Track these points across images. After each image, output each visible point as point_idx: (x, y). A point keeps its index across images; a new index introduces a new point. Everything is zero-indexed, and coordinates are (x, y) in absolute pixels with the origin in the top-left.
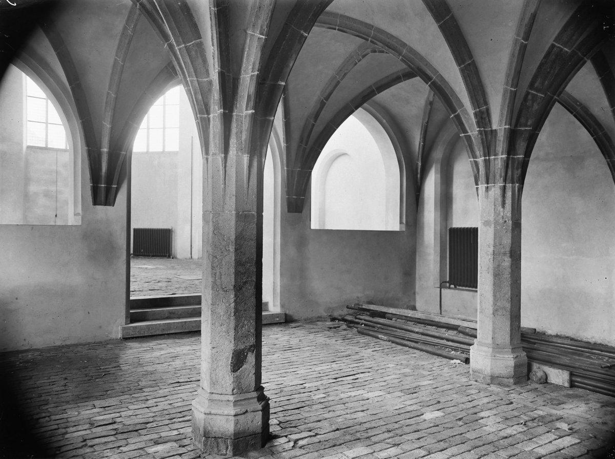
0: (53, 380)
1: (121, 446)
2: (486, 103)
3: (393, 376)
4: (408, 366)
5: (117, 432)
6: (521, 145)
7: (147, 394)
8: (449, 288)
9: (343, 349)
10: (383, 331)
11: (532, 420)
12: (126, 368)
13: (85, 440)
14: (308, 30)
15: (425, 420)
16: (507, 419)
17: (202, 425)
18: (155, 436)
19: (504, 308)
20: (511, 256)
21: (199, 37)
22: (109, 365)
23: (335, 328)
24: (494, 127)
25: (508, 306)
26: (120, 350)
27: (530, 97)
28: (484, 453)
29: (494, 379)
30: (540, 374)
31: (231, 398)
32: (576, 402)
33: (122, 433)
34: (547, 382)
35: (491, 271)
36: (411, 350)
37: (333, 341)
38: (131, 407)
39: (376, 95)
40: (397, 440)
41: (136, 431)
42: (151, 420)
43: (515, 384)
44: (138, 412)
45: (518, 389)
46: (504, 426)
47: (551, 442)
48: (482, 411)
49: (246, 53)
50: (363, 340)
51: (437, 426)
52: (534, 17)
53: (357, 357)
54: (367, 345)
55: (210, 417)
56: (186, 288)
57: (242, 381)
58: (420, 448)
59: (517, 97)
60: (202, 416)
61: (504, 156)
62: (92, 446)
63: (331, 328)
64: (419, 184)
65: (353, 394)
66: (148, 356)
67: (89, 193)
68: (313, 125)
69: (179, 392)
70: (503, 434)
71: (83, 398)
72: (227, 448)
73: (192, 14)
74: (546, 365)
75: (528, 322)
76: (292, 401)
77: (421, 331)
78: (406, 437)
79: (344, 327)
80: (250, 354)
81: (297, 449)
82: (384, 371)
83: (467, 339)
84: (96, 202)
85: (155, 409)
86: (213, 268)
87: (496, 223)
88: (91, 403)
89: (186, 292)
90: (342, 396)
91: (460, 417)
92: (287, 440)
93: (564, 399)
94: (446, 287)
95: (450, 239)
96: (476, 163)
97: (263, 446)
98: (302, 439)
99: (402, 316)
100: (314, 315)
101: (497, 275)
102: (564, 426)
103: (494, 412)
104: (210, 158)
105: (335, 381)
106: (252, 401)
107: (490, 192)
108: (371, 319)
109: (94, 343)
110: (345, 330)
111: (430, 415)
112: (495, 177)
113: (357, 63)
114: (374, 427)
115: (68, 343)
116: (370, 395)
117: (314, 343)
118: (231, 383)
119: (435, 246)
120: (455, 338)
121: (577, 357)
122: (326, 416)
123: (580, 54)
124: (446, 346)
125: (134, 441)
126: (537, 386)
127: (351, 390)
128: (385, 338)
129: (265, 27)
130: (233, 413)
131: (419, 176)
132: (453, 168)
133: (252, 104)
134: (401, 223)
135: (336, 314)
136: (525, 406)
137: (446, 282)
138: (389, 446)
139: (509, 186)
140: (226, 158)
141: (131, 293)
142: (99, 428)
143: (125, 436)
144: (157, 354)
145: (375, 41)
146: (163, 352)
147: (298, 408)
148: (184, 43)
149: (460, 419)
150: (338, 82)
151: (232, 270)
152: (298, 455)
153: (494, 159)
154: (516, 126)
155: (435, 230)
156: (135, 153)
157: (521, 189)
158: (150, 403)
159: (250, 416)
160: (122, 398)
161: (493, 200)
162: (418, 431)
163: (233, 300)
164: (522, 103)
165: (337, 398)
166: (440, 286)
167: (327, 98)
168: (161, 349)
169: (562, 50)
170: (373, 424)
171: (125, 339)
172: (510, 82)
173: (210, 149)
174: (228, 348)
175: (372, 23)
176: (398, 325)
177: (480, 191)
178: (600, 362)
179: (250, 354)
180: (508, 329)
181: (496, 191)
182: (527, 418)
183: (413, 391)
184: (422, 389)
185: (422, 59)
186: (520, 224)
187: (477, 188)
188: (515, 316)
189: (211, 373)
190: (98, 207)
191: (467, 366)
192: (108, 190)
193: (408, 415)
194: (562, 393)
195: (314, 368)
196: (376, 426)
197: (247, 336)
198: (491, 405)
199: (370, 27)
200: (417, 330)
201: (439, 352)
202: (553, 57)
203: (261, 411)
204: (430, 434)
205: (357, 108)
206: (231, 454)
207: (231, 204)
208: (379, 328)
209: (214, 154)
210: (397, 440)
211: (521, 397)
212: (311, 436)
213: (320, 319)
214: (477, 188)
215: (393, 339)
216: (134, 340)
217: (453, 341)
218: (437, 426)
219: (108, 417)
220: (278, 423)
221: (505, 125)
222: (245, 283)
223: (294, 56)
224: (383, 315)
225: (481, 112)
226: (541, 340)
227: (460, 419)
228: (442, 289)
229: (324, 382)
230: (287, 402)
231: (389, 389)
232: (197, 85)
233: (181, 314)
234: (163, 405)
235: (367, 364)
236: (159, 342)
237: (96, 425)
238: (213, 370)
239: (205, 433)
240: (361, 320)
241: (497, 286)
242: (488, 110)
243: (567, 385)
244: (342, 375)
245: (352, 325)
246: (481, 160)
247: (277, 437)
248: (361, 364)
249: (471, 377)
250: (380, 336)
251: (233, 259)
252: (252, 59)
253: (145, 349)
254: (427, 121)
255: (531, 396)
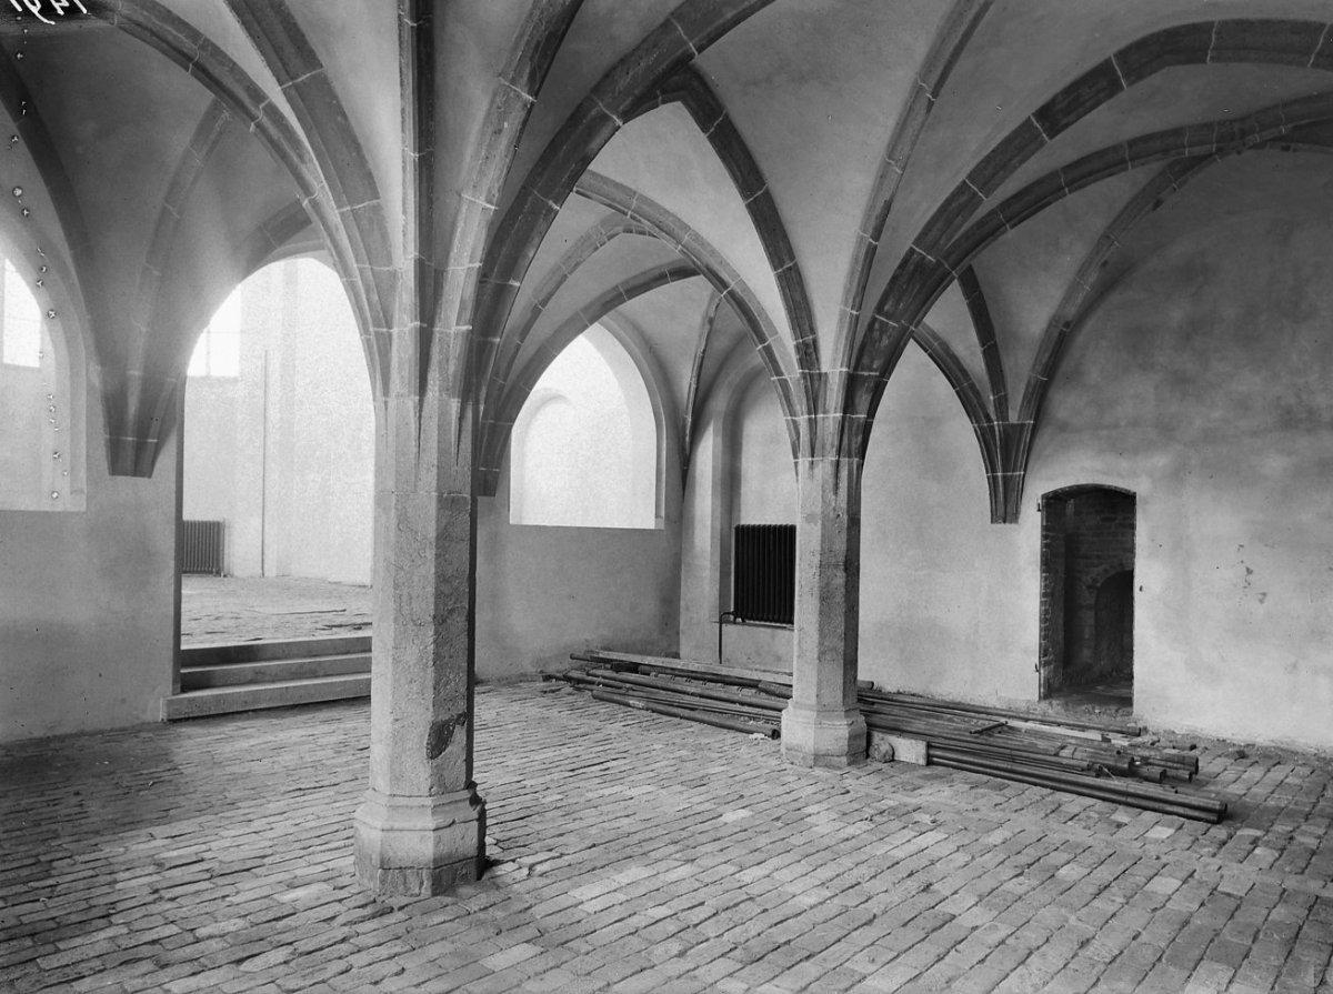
0: (52, 797)
1: (228, 896)
2: (813, 330)
3: (663, 763)
4: (684, 746)
5: (212, 876)
6: (863, 400)
7: (247, 811)
8: (735, 623)
9: (574, 724)
10: (635, 693)
11: (881, 813)
12: (190, 771)
13: (156, 891)
14: (561, 200)
15: (726, 824)
16: (845, 814)
17: (378, 850)
18: (287, 876)
19: (834, 649)
20: (846, 570)
21: (376, 196)
22: (157, 767)
23: (553, 691)
24: (824, 370)
25: (841, 646)
26: (169, 741)
27: (877, 326)
28: (820, 862)
29: (819, 759)
30: (884, 748)
31: (429, 802)
32: (937, 786)
33: (222, 875)
34: (893, 760)
35: (816, 591)
36: (685, 722)
37: (555, 712)
38: (225, 833)
39: (625, 301)
40: (690, 853)
41: (248, 870)
42: (269, 851)
43: (849, 764)
44: (240, 840)
45: (855, 771)
46: (842, 825)
47: (909, 841)
48: (807, 805)
49: (459, 230)
50: (603, 709)
51: (745, 830)
52: (888, 206)
53: (600, 736)
54: (611, 718)
55: (391, 834)
56: (276, 629)
57: (445, 773)
58: (725, 863)
59: (860, 322)
60: (376, 836)
61: (839, 415)
62: (173, 899)
63: (545, 692)
64: (688, 452)
65: (606, 792)
66: (227, 749)
67: (101, 453)
68: (518, 348)
69: (305, 804)
70: (843, 835)
71: (124, 825)
72: (422, 883)
73: (363, 157)
74: (893, 734)
75: (863, 675)
76: (509, 809)
77: (699, 691)
78: (703, 849)
79: (568, 689)
80: (458, 727)
81: (536, 879)
82: (646, 755)
83: (773, 701)
84: (116, 468)
85: (270, 834)
86: (396, 586)
87: (825, 517)
88: (144, 832)
89: (280, 635)
90: (590, 795)
91: (776, 815)
92: (515, 866)
93: (921, 782)
94: (728, 622)
95: (737, 547)
96: (795, 425)
97: (479, 878)
98: (541, 862)
99: (666, 668)
100: (513, 672)
101: (825, 598)
102: (926, 819)
103: (825, 805)
104: (392, 403)
105: (571, 774)
106: (461, 805)
107: (816, 471)
108: (615, 675)
109: (111, 730)
110: (570, 694)
111: (732, 816)
112: (823, 448)
113: (597, 248)
114: (651, 839)
115: (60, 731)
116: (633, 792)
117: (523, 718)
118: (426, 776)
119: (712, 554)
120: (754, 700)
121: (936, 722)
122: (571, 826)
123: (946, 266)
124: (741, 714)
125: (248, 886)
126: (880, 766)
127: (602, 786)
128: (641, 705)
129: (495, 192)
130: (432, 825)
131: (687, 439)
132: (742, 425)
133: (468, 314)
134: (657, 516)
135: (551, 669)
136: (867, 795)
137: (729, 613)
138: (680, 863)
139: (844, 461)
140: (421, 402)
141: (183, 638)
142: (175, 870)
143: (229, 879)
144: (245, 744)
145: (639, 218)
146: (252, 742)
147: (522, 818)
148: (350, 203)
149: (778, 819)
150: (565, 277)
151: (431, 590)
152: (540, 886)
153: (824, 419)
154: (856, 369)
155: (713, 528)
156: (193, 378)
157: (860, 466)
158: (256, 825)
159: (458, 830)
160: (202, 819)
161: (820, 481)
162: (719, 839)
163: (431, 640)
164: (865, 335)
165: (582, 800)
166: (721, 620)
167: (544, 302)
168: (248, 737)
169: (924, 258)
170: (647, 834)
171: (174, 721)
172: (851, 301)
173: (392, 386)
174: (422, 718)
175: (633, 187)
176: (659, 684)
177: (800, 468)
178: (966, 725)
179: (458, 727)
180: (840, 681)
181: (824, 468)
182: (872, 812)
183: (701, 782)
184: (713, 778)
185: (713, 252)
186: (859, 520)
187: (796, 464)
188: (850, 663)
189: (392, 761)
190: (120, 478)
191: (776, 742)
192: (140, 447)
193: (699, 818)
194: (916, 774)
195: (533, 756)
196: (653, 836)
197: (453, 700)
198: (819, 797)
199: (631, 193)
200: (693, 690)
201: (729, 723)
202: (912, 268)
203: (477, 820)
204: (739, 842)
205: (592, 323)
206: (429, 893)
207: (429, 479)
208: (628, 689)
209: (399, 396)
210: (690, 853)
211: (861, 782)
212: (554, 858)
213: (524, 678)
214: (796, 464)
215: (651, 705)
216: (201, 721)
217: (750, 705)
218: (745, 830)
219: (188, 852)
220: (495, 842)
221: (841, 366)
222: (451, 612)
223: (536, 240)
224: (634, 668)
225: (806, 345)
226: (882, 699)
227: (778, 819)
228: (724, 625)
229: (556, 776)
230: (502, 811)
231: (662, 782)
232: (371, 278)
233: (276, 675)
234: (282, 827)
235: (621, 746)
236: (240, 724)
237: (167, 866)
238: (395, 760)
239: (382, 862)
240: (598, 676)
241: (824, 614)
242: (815, 341)
243: (922, 761)
244: (583, 764)
245: (581, 686)
246: (803, 419)
247: (497, 863)
248: (610, 746)
249: (784, 757)
250: (631, 702)
251: (433, 570)
252: (470, 240)
253: (218, 737)
254: (704, 350)
255: (874, 779)
